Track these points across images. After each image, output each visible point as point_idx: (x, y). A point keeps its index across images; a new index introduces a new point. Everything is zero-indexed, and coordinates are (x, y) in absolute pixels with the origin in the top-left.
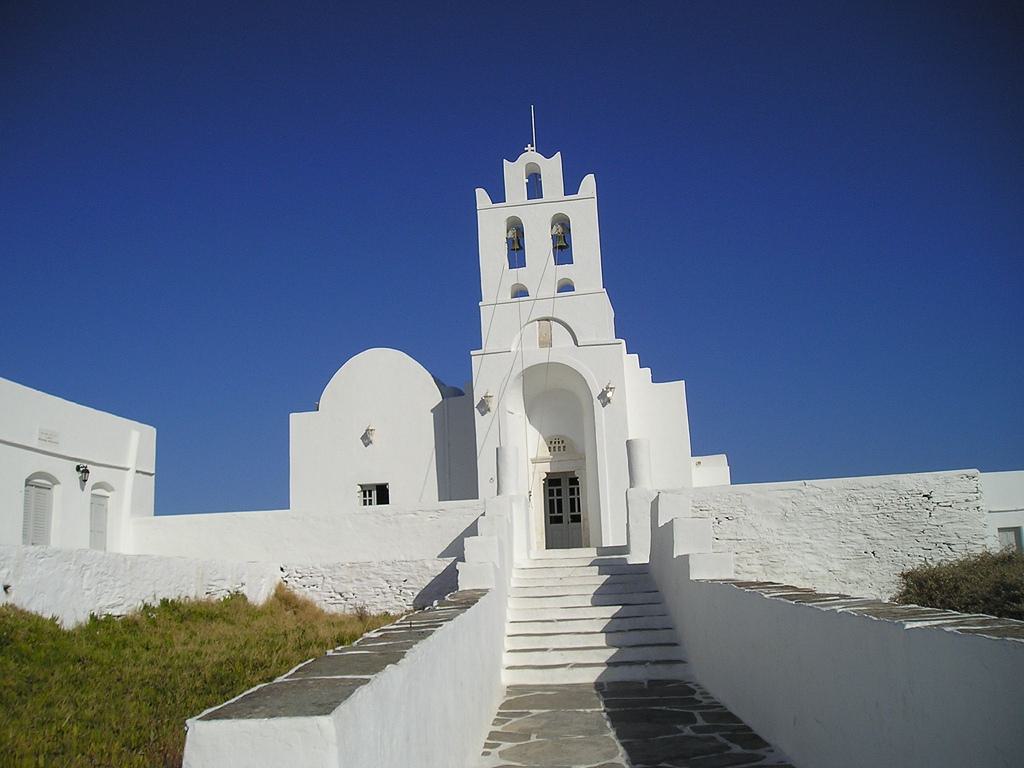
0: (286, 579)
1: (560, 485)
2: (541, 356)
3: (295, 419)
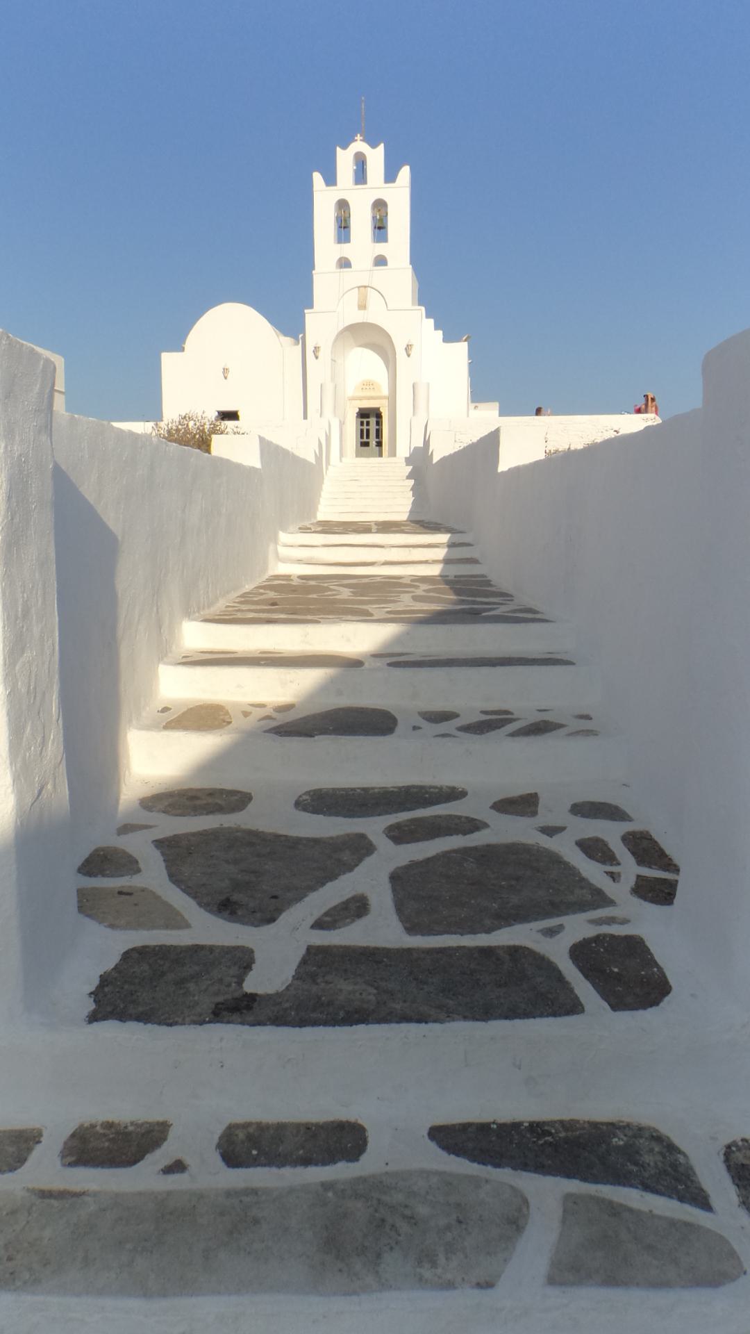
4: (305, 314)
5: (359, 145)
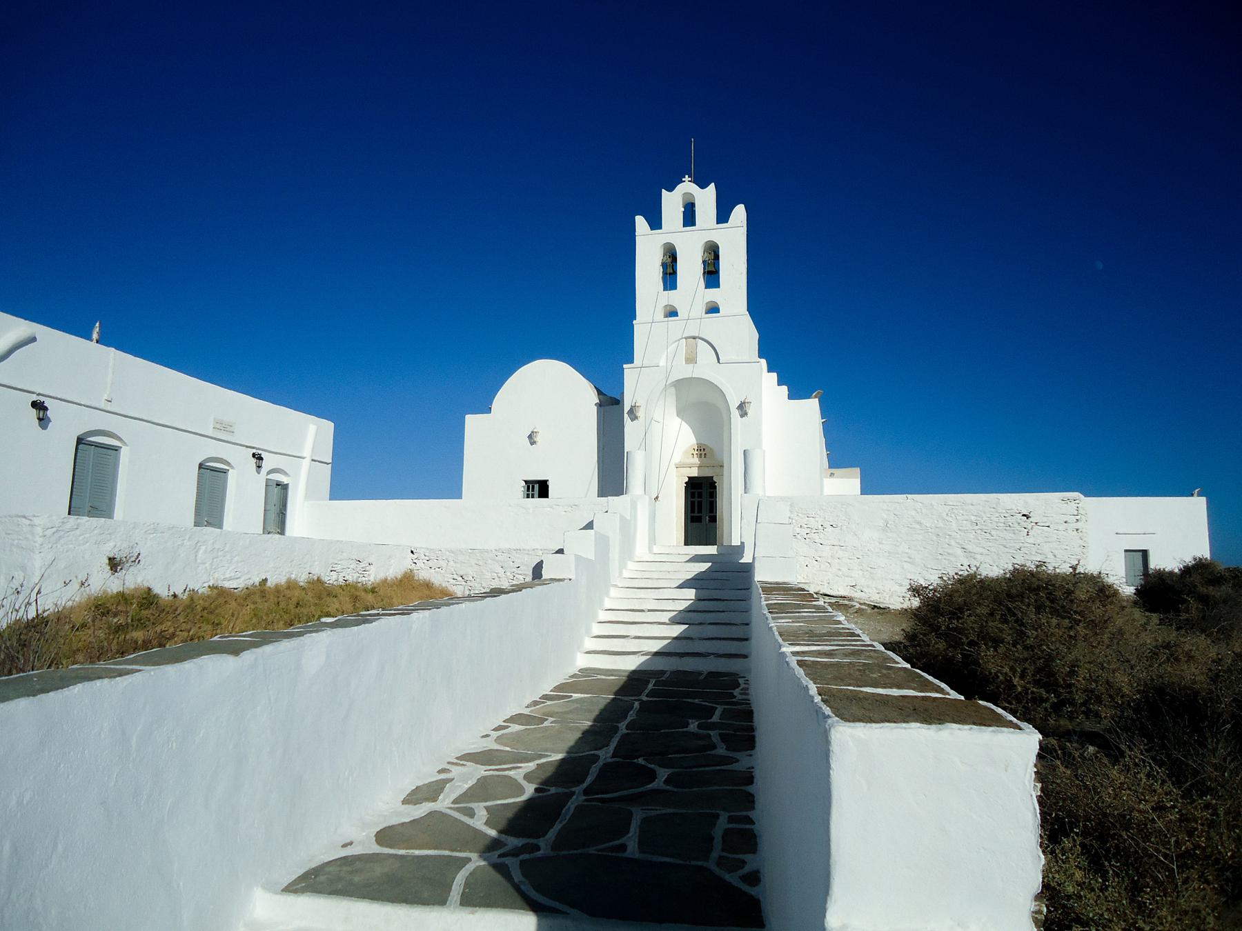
0: (415, 561)
1: (701, 488)
3: (473, 422)
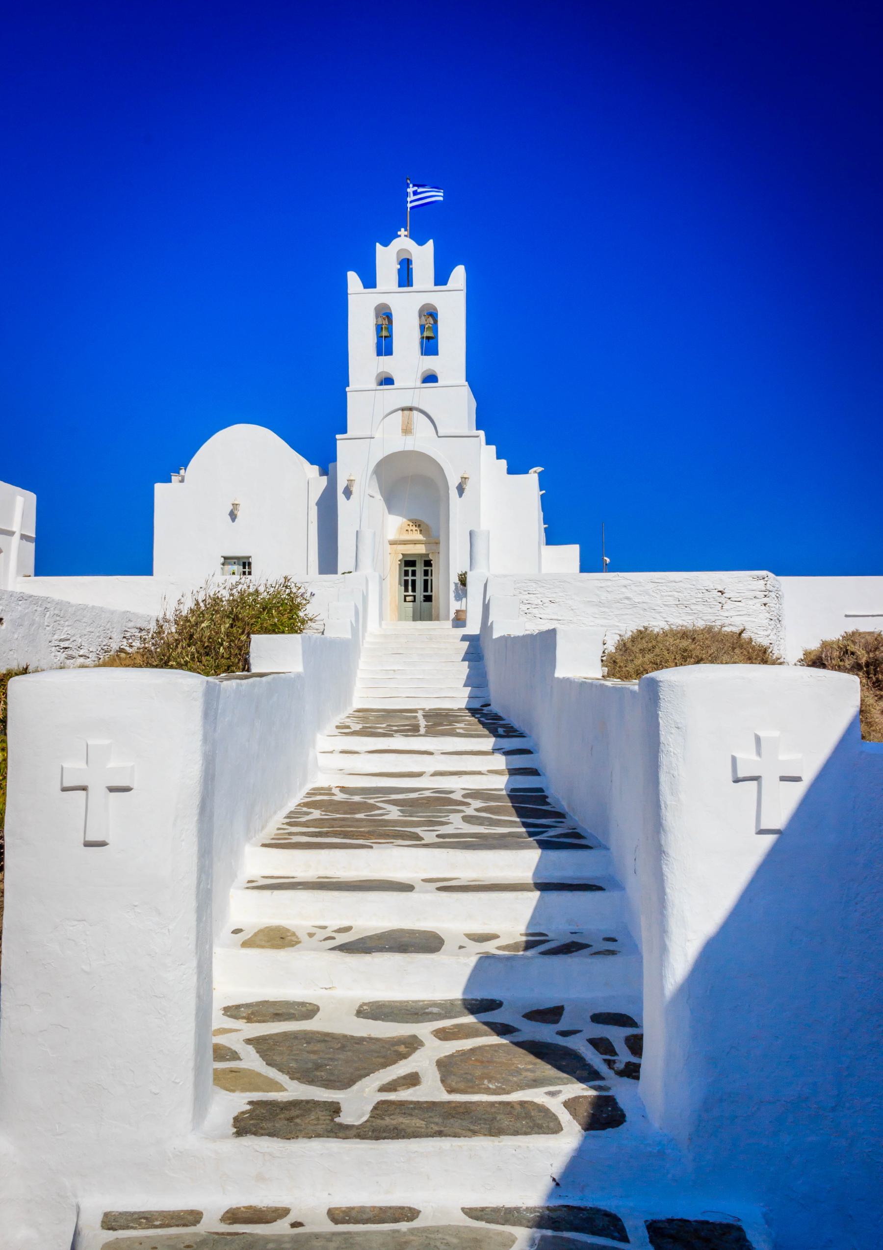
2: (399, 443)
4: (336, 440)
5: (403, 242)
